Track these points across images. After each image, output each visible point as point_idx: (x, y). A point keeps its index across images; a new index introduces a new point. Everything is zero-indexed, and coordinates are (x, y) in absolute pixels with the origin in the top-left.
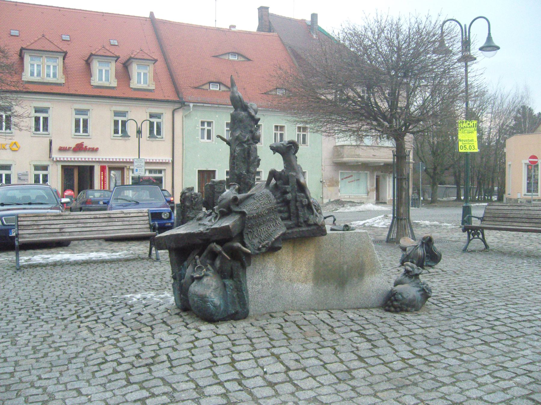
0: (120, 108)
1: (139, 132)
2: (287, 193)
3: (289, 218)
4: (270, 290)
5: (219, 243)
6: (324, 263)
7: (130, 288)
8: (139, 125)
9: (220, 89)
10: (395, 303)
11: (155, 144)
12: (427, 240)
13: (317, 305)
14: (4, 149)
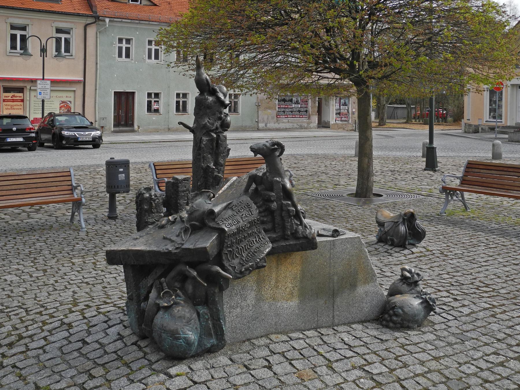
0: (19, 21)
1: (43, 50)
2: (272, 202)
3: (274, 230)
4: (251, 313)
5: (193, 265)
7: (56, 282)
8: (44, 42)
9: (141, 3)
10: (395, 318)
11: (63, 63)
12: (408, 215)
13: (304, 324)
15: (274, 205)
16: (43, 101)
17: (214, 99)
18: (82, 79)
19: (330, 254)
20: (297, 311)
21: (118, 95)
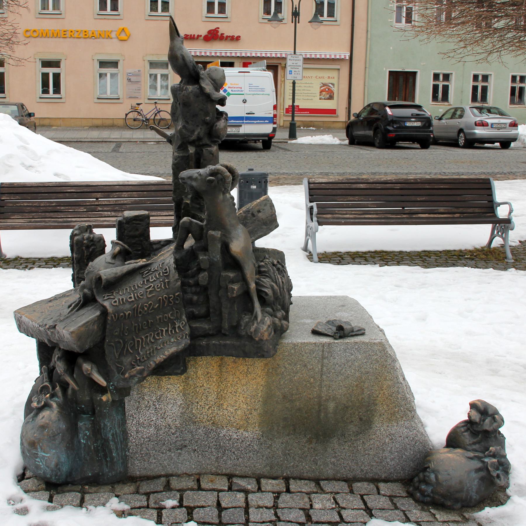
1: (296, 14)
6: (284, 397)
11: (323, 30)
13: (268, 468)
14: (109, 37)
15: (203, 277)
16: (294, 83)
17: (196, 90)
18: (348, 55)
19: (322, 366)
20: (255, 447)
21: (394, 76)
